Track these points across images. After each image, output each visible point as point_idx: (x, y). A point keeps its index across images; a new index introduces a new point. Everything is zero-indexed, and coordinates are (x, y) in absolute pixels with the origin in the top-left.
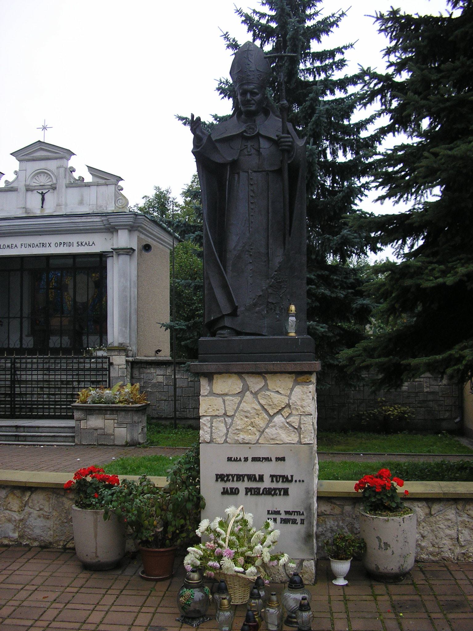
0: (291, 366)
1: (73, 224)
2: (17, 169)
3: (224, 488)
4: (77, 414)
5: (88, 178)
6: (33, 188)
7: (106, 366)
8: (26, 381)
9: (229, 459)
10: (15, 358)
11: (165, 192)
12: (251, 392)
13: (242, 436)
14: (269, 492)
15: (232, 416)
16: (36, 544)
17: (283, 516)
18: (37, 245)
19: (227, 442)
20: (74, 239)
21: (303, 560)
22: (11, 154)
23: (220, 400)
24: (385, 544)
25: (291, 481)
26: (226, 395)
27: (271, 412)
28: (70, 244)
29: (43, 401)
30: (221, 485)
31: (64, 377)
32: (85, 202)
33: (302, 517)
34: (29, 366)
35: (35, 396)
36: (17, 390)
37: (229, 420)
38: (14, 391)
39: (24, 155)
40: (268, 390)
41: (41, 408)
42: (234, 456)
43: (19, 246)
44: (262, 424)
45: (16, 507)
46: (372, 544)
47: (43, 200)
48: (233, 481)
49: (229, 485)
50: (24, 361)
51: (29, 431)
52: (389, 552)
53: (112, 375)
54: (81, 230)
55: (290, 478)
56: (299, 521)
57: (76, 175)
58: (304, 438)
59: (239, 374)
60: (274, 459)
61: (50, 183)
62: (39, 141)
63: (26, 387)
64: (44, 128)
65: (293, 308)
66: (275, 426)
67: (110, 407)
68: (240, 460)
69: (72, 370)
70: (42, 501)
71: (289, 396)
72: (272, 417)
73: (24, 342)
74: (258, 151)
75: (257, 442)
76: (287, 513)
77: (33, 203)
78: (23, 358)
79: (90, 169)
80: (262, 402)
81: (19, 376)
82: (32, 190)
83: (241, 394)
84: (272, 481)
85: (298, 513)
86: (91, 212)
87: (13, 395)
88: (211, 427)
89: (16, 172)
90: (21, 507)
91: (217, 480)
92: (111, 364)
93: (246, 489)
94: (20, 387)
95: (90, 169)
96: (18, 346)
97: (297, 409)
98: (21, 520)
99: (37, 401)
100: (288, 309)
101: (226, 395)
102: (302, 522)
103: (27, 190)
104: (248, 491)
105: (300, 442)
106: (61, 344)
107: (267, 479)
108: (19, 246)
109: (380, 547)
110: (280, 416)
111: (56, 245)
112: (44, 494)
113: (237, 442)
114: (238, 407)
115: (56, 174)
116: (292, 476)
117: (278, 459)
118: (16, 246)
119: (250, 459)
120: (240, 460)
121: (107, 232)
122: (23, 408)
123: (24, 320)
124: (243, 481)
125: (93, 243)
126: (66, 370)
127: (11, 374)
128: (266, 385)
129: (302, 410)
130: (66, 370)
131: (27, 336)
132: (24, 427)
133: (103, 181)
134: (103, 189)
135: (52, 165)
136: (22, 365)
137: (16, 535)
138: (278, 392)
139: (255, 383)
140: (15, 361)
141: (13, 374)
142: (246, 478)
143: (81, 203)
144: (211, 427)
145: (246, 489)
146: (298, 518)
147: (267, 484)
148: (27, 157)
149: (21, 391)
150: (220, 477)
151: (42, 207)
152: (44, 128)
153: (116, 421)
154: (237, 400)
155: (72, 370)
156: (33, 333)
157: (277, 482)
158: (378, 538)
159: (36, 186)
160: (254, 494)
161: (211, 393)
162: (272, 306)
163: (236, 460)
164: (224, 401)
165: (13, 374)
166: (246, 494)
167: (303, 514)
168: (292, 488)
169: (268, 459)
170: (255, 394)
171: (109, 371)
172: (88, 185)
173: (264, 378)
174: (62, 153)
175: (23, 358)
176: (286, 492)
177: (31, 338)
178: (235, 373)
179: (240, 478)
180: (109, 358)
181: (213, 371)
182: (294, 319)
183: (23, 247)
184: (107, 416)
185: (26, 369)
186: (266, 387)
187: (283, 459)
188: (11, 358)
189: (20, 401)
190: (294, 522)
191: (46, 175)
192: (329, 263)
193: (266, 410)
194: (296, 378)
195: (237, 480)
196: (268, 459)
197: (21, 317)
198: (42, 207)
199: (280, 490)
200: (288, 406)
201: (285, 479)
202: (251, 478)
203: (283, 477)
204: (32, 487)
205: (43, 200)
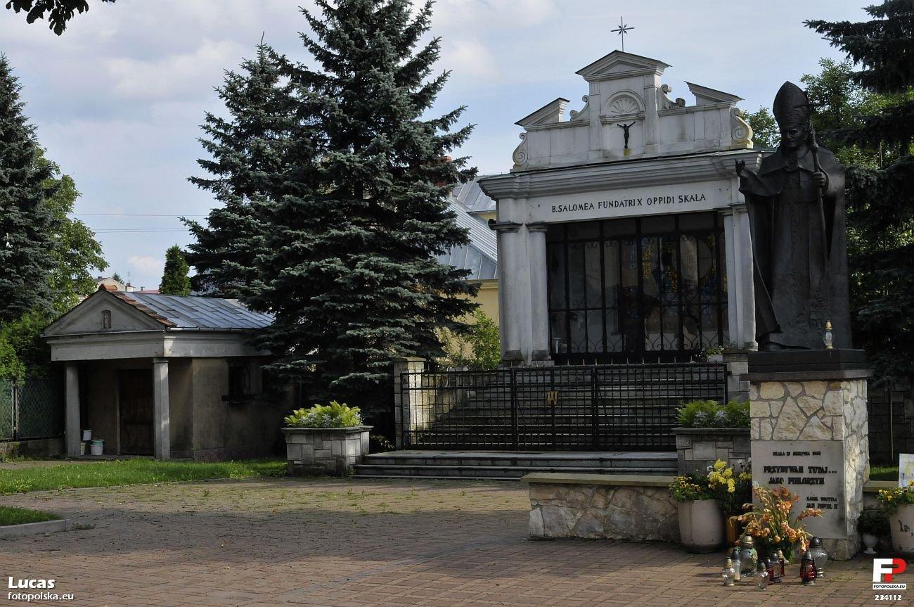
0: (822, 375)
1: (672, 167)
2: (588, 94)
3: (771, 478)
4: (680, 442)
5: (691, 101)
6: (611, 120)
7: (721, 376)
8: (613, 401)
9: (775, 454)
10: (597, 368)
11: (840, 68)
12: (792, 397)
13: (785, 435)
14: (807, 481)
15: (777, 417)
16: (620, 537)
17: (820, 502)
18: (622, 204)
19: (773, 439)
20: (674, 191)
21: (837, 540)
22: (576, 73)
23: (767, 404)
24: (906, 526)
25: (826, 472)
26: (772, 400)
27: (809, 415)
28: (669, 200)
29: (637, 427)
30: (768, 476)
31: (664, 395)
32: (687, 137)
33: (835, 503)
34: (616, 380)
35: (626, 420)
36: (601, 414)
37: (774, 421)
38: (597, 414)
39: (595, 72)
40: (805, 395)
41: (633, 436)
42: (778, 451)
43: (596, 206)
44: (801, 424)
45: (601, 504)
46: (895, 527)
47: (627, 136)
48: (778, 472)
49: (775, 475)
50: (609, 371)
51: (617, 465)
52: (908, 534)
53: (730, 389)
54: (683, 178)
55: (825, 470)
56: (833, 506)
57: (672, 97)
58: (836, 435)
59: (781, 381)
60: (811, 454)
61: (635, 112)
62: (616, 51)
63: (613, 408)
64: (622, 30)
65: (829, 324)
66: (811, 426)
67: (721, 431)
68: (784, 454)
69: (675, 383)
70: (624, 500)
71: (823, 400)
72: (809, 418)
73: (609, 344)
74: (798, 183)
75: (798, 440)
76: (823, 499)
77: (611, 140)
78: (624, 367)
79: (694, 88)
80: (801, 405)
81: (603, 393)
82: (610, 123)
83: (784, 399)
84: (810, 472)
85: (832, 499)
86: (696, 150)
87: (595, 420)
88: (760, 427)
89: (585, 98)
90: (606, 504)
91: (765, 471)
92: (729, 373)
93: (789, 478)
94: (605, 408)
95: (694, 88)
96: (601, 351)
97: (829, 411)
98: (605, 516)
99: (629, 427)
100: (825, 325)
101: (772, 400)
102: (836, 507)
103: (604, 123)
104: (791, 480)
105: (832, 439)
106: (662, 345)
107: (806, 470)
108: (596, 206)
109: (902, 530)
110: (816, 417)
111: (650, 202)
112: (626, 492)
113: (781, 440)
114: (781, 410)
115: (643, 97)
116: (826, 468)
117: (815, 453)
118: (591, 206)
119: (792, 454)
120: (784, 454)
121: (722, 179)
122: (610, 436)
123: (607, 311)
124: (787, 472)
125: (703, 197)
126: (667, 383)
127: (592, 391)
128: (804, 390)
129: (834, 412)
130: (667, 383)
131: (612, 334)
132: (611, 460)
133: (712, 104)
134: (713, 115)
135: (636, 85)
136: (607, 377)
137: (601, 530)
138: (813, 397)
139: (795, 389)
140: (596, 372)
141: (595, 391)
142: (789, 469)
143: (682, 137)
144: (760, 427)
145: (789, 478)
146: (832, 504)
147: (806, 474)
148: (599, 76)
149: (606, 414)
150: (768, 469)
151: (626, 147)
152: (622, 30)
153: (731, 450)
154: (780, 403)
155: (675, 383)
156: (621, 330)
157: (815, 472)
158: (899, 521)
159: (614, 117)
160: (796, 483)
161: (759, 399)
162: (815, 322)
163: (780, 454)
164: (770, 405)
165: (595, 391)
166: (789, 483)
167: (836, 500)
168: (827, 477)
169: (806, 454)
170: (795, 399)
171: (726, 383)
172: (691, 111)
173: (802, 385)
174: (650, 66)
175: (624, 367)
176: (822, 481)
177: (619, 337)
178: (778, 381)
179: (784, 469)
180: (726, 365)
181: (760, 380)
182: (831, 334)
183: (602, 207)
184: (720, 444)
185: (612, 384)
186: (803, 393)
187: (819, 453)
188: (591, 368)
189: (606, 427)
190: (829, 507)
191: (629, 100)
192: (648, 349)
193: (803, 412)
194: (829, 384)
195: (782, 471)
196: (806, 454)
197: (604, 308)
198: (626, 147)
199: (817, 479)
200: (822, 408)
201: (821, 470)
202: (793, 469)
203: (819, 468)
204: (616, 486)
205: (627, 136)
